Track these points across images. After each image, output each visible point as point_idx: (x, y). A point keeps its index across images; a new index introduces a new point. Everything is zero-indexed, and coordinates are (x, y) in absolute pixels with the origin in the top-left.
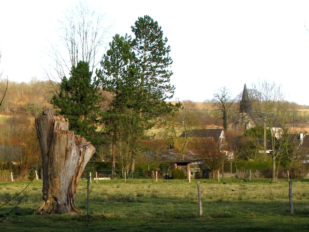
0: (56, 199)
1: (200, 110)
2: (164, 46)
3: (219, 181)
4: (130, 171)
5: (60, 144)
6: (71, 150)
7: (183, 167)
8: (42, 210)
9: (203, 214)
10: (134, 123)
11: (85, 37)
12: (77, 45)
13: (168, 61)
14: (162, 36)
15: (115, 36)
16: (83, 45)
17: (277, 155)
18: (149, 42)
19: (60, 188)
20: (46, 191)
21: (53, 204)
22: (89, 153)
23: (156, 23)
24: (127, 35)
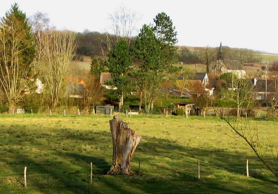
0: (120, 165)
2: (173, 32)
3: (205, 118)
4: (151, 108)
6: (129, 139)
8: (112, 171)
9: (200, 178)
10: (154, 79)
11: (125, 24)
16: (123, 29)
17: (240, 104)
23: (169, 17)
24: (150, 23)
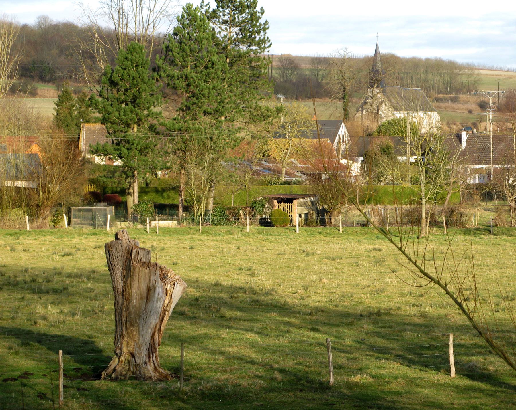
0: (133, 356)
1: (306, 75)
2: (260, 21)
3: (341, 232)
4: (207, 211)
5: (140, 281)
7: (289, 205)
8: (114, 370)
10: (214, 139)
11: (138, 4)
12: (126, 15)
13: (265, 43)
14: (256, 6)
15: (186, 6)
17: (429, 196)
18: (237, 13)
19: (139, 340)
20: (119, 343)
21: (129, 362)
22: (179, 291)
24: (203, 2)
